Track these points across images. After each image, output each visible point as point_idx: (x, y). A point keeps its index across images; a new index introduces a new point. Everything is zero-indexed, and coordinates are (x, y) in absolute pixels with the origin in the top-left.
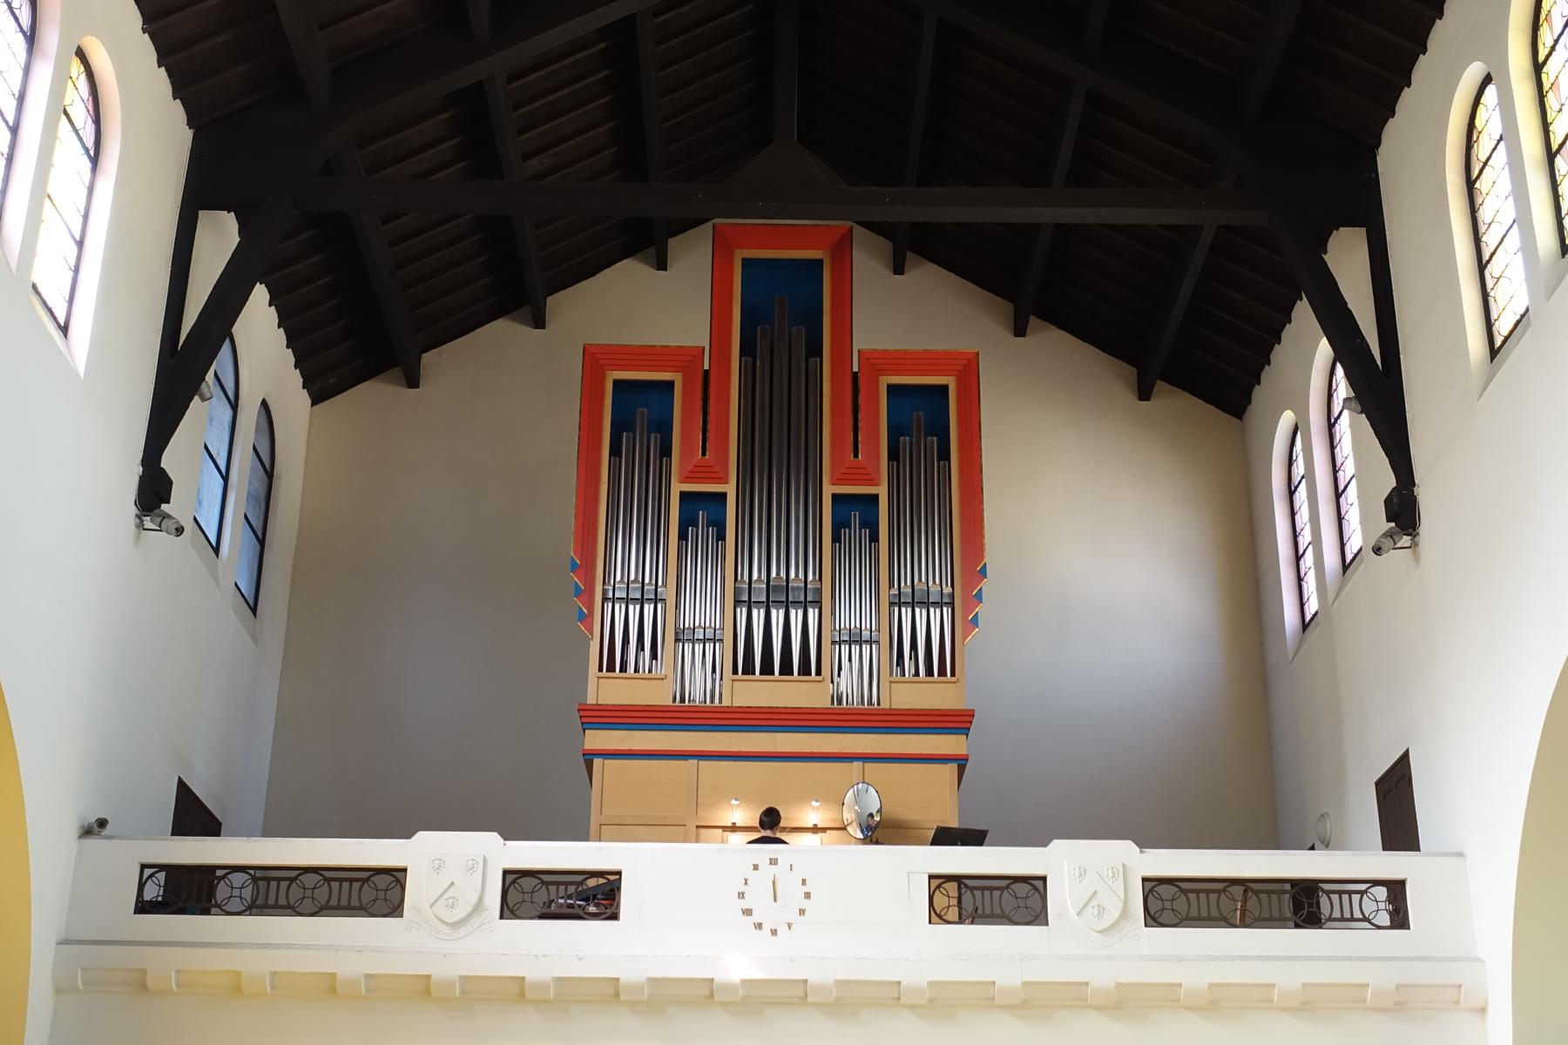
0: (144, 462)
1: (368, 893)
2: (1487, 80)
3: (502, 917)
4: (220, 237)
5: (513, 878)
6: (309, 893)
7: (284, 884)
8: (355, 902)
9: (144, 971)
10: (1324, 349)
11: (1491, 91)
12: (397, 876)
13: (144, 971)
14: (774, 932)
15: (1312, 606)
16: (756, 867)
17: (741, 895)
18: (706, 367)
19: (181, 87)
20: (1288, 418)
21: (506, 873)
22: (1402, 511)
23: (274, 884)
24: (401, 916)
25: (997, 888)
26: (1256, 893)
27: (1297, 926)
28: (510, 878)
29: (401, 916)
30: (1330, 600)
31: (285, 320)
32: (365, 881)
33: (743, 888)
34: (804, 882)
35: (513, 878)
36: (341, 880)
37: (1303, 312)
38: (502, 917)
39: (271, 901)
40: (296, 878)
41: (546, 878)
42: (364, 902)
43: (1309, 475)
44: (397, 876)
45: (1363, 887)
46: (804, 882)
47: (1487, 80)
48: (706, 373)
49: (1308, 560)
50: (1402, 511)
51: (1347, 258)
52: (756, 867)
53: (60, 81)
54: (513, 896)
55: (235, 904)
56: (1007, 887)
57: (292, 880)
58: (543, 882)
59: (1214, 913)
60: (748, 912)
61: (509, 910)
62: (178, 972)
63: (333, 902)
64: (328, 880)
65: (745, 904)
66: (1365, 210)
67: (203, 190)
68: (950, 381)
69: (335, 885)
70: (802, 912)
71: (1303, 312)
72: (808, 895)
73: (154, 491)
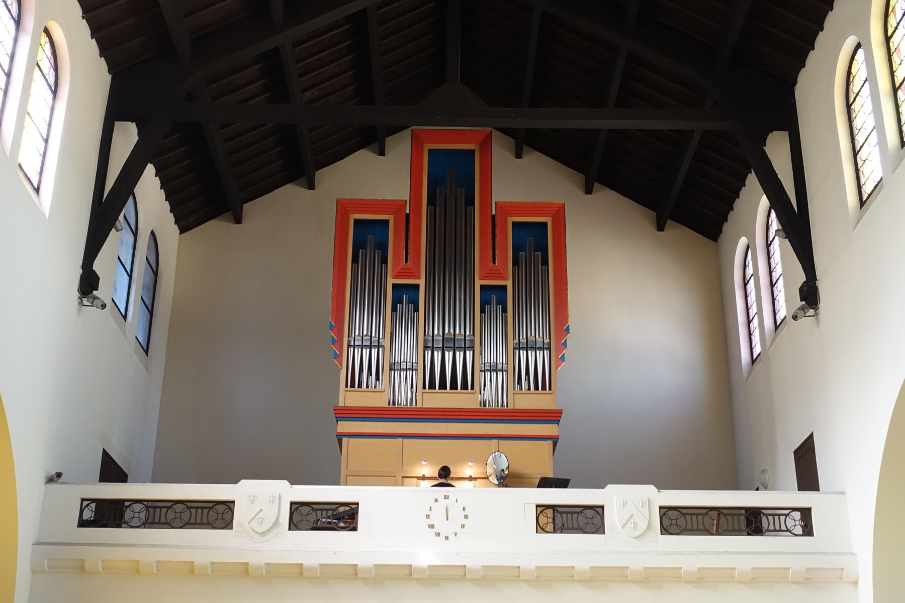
0: (83, 267)
1: (212, 515)
2: (859, 46)
3: (289, 529)
4: (127, 137)
5: (296, 507)
6: (178, 515)
7: (164, 510)
8: (205, 521)
9: (83, 560)
10: (764, 202)
11: (860, 52)
12: (229, 505)
13: (83, 560)
14: (447, 538)
15: (757, 350)
16: (436, 500)
17: (428, 517)
18: (408, 212)
19: (105, 50)
20: (743, 241)
21: (292, 503)
22: (809, 295)
23: (158, 510)
24: (232, 528)
25: (576, 513)
26: (725, 515)
27: (749, 534)
28: (294, 507)
29: (232, 528)
30: (768, 346)
31: (165, 185)
32: (211, 508)
33: (429, 513)
34: (464, 509)
35: (296, 507)
36: (197, 508)
37: (752, 180)
38: (289, 529)
39: (157, 520)
40: (171, 507)
41: (315, 507)
42: (210, 520)
43: (756, 274)
44: (229, 505)
45: (787, 512)
46: (464, 509)
47: (859, 46)
48: (408, 215)
49: (755, 323)
50: (809, 295)
51: (777, 149)
52: (436, 500)
53: (35, 46)
54: (296, 517)
55: (136, 522)
56: (581, 512)
57: (168, 508)
58: (313, 509)
59: (701, 527)
60: (432, 526)
61: (294, 525)
62: (102, 561)
63: (192, 521)
64: (189, 508)
65: (430, 522)
66: (788, 121)
67: (117, 110)
68: (548, 220)
69: (193, 511)
70: (463, 526)
71: (752, 180)
72: (466, 517)
73: (89, 283)
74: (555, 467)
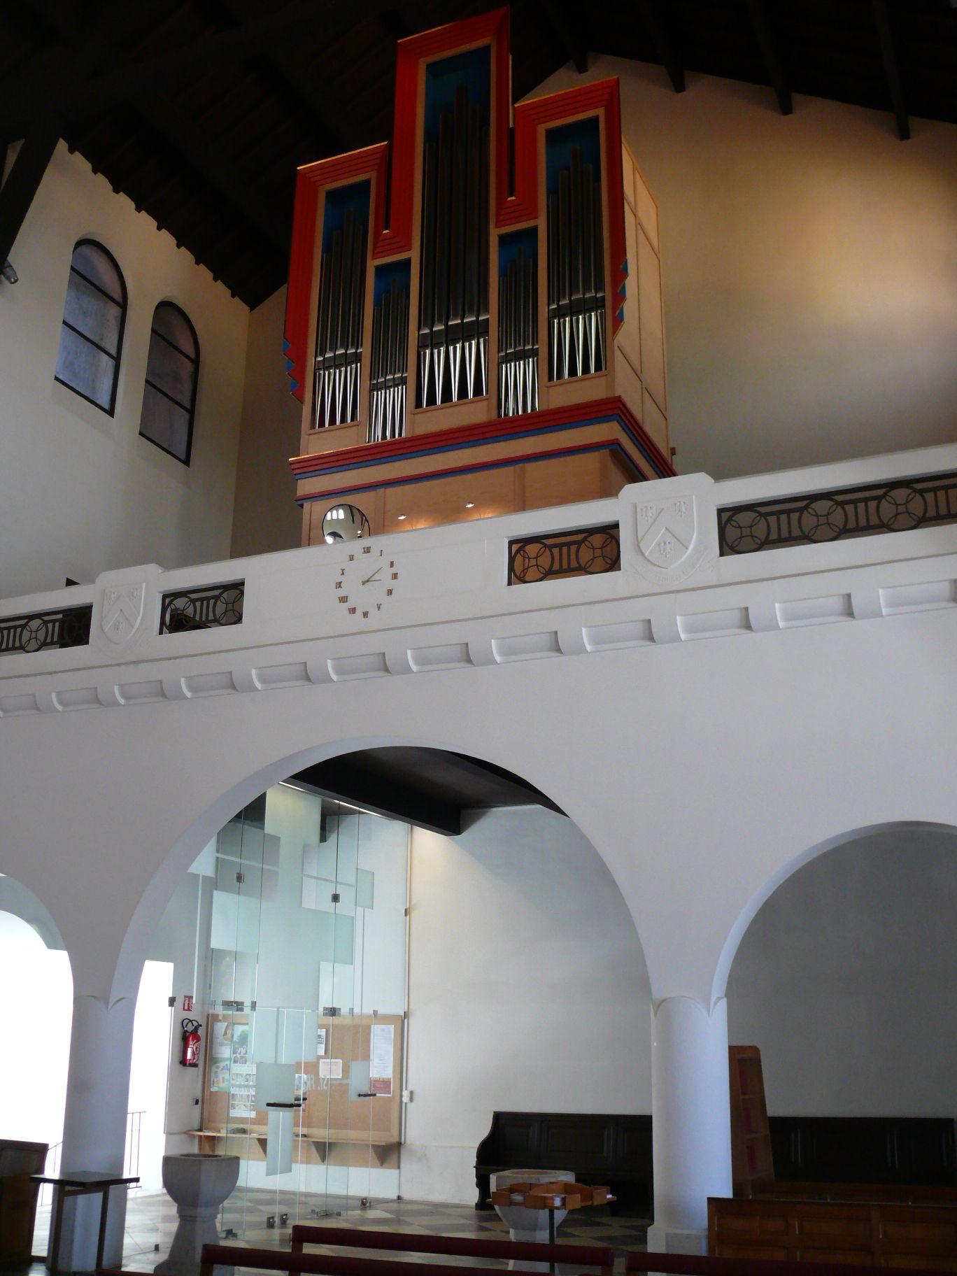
3: (722, 554)
5: (519, 546)
6: (746, 532)
8: (574, 564)
9: (161, 682)
12: (610, 531)
13: (161, 682)
14: (365, 614)
17: (339, 585)
21: (720, 511)
23: (565, 549)
24: (87, 643)
25: (794, 510)
26: (842, 504)
27: (61, 647)
28: (725, 516)
29: (87, 643)
33: (340, 578)
35: (519, 546)
36: (854, 502)
38: (722, 554)
39: (565, 566)
40: (26, 624)
41: (763, 510)
42: (583, 563)
44: (610, 531)
45: (23, 622)
54: (732, 533)
55: (532, 573)
56: (885, 495)
58: (915, 490)
59: (796, 532)
60: (343, 600)
62: (58, 693)
63: (774, 536)
64: (765, 515)
65: (341, 593)
68: (542, 130)
70: (390, 592)
72: (395, 576)
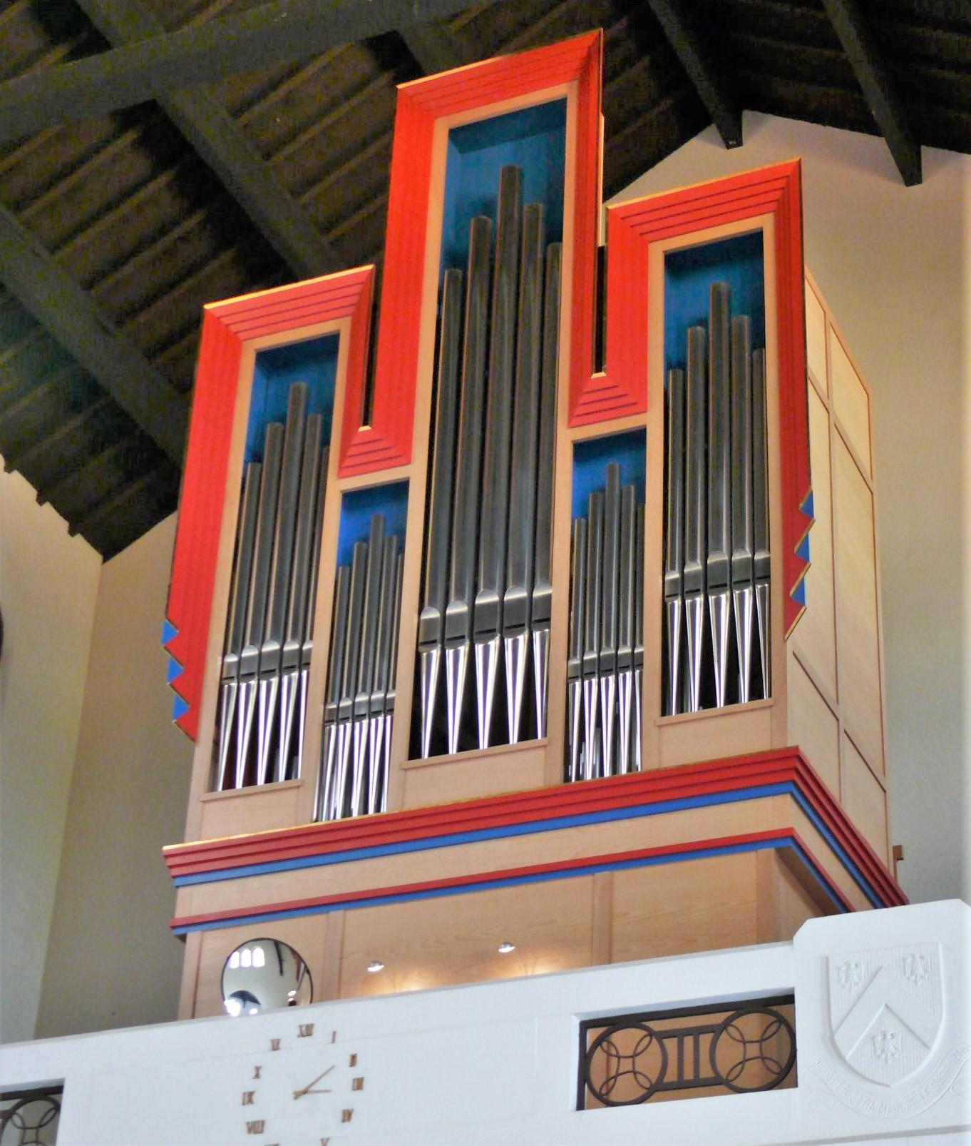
1: (728, 1053)
5: (601, 1031)
7: (705, 1040)
12: (776, 1008)
16: (276, 1045)
17: (249, 1098)
18: (601, 242)
32: (717, 1030)
33: (251, 1085)
34: (353, 1060)
38: (580, 1106)
44: (776, 1008)
46: (353, 1060)
48: (601, 252)
52: (276, 1045)
57: (717, 1030)
58: (651, 1033)
61: (594, 1091)
63: (671, 1076)
64: (661, 1036)
65: (253, 1113)
68: (765, 223)
69: (671, 1044)
70: (347, 1115)
72: (359, 1084)
74: (953, 894)
